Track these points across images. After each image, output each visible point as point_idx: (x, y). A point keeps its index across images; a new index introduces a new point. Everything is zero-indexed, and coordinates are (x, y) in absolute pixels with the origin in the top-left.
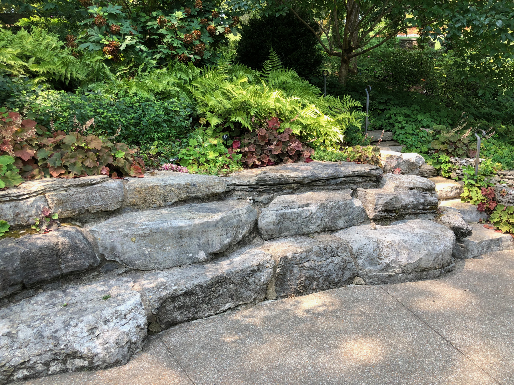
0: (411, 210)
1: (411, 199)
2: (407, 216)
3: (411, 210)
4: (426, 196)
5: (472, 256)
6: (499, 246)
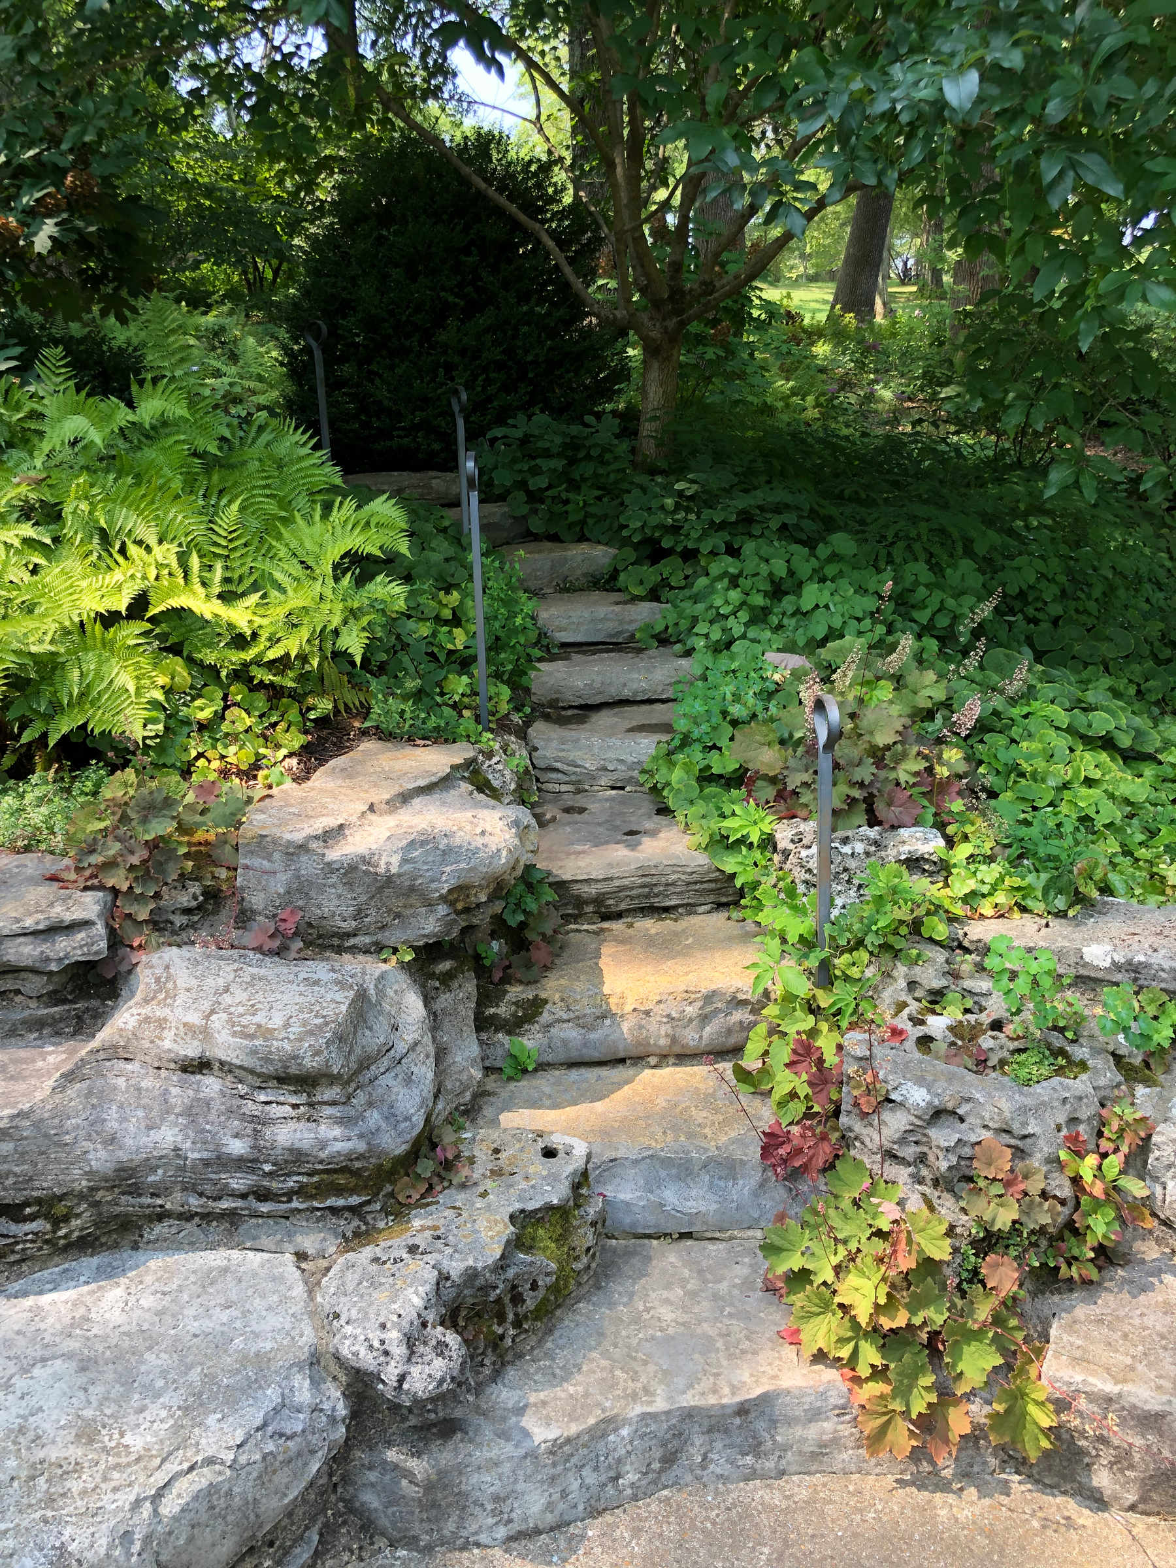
0: (178, 1196)
1: (168, 1136)
2: (160, 1229)
3: (178, 1196)
4: (264, 1121)
5: (501, 1532)
6: (755, 1448)
